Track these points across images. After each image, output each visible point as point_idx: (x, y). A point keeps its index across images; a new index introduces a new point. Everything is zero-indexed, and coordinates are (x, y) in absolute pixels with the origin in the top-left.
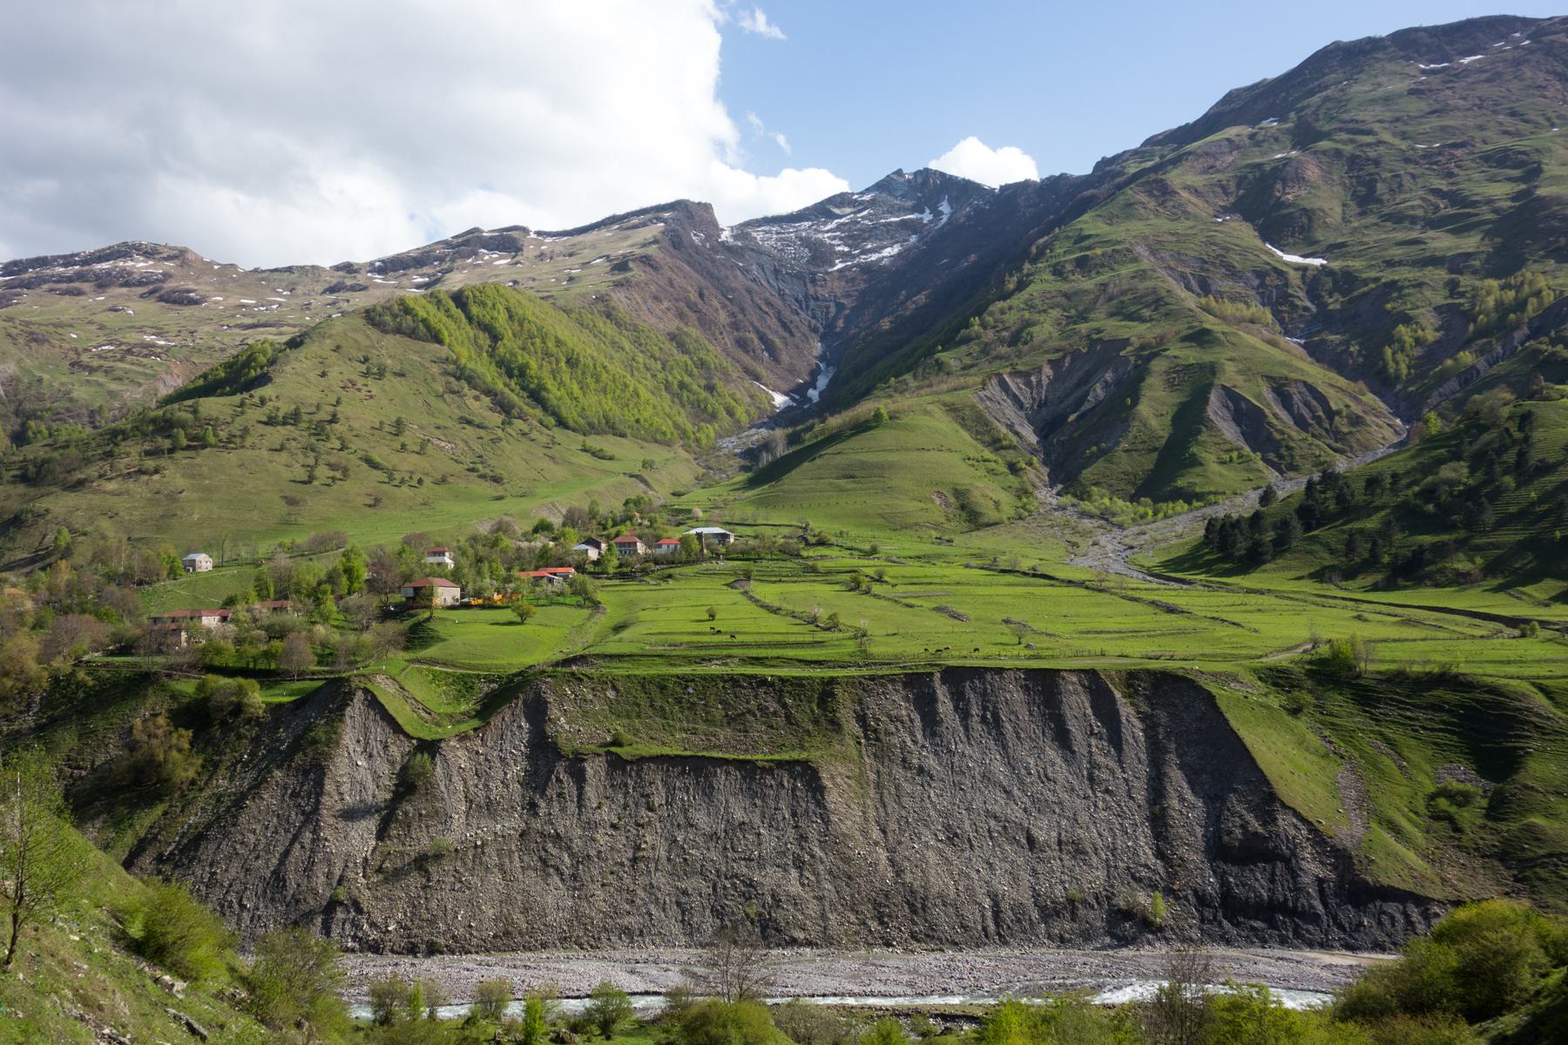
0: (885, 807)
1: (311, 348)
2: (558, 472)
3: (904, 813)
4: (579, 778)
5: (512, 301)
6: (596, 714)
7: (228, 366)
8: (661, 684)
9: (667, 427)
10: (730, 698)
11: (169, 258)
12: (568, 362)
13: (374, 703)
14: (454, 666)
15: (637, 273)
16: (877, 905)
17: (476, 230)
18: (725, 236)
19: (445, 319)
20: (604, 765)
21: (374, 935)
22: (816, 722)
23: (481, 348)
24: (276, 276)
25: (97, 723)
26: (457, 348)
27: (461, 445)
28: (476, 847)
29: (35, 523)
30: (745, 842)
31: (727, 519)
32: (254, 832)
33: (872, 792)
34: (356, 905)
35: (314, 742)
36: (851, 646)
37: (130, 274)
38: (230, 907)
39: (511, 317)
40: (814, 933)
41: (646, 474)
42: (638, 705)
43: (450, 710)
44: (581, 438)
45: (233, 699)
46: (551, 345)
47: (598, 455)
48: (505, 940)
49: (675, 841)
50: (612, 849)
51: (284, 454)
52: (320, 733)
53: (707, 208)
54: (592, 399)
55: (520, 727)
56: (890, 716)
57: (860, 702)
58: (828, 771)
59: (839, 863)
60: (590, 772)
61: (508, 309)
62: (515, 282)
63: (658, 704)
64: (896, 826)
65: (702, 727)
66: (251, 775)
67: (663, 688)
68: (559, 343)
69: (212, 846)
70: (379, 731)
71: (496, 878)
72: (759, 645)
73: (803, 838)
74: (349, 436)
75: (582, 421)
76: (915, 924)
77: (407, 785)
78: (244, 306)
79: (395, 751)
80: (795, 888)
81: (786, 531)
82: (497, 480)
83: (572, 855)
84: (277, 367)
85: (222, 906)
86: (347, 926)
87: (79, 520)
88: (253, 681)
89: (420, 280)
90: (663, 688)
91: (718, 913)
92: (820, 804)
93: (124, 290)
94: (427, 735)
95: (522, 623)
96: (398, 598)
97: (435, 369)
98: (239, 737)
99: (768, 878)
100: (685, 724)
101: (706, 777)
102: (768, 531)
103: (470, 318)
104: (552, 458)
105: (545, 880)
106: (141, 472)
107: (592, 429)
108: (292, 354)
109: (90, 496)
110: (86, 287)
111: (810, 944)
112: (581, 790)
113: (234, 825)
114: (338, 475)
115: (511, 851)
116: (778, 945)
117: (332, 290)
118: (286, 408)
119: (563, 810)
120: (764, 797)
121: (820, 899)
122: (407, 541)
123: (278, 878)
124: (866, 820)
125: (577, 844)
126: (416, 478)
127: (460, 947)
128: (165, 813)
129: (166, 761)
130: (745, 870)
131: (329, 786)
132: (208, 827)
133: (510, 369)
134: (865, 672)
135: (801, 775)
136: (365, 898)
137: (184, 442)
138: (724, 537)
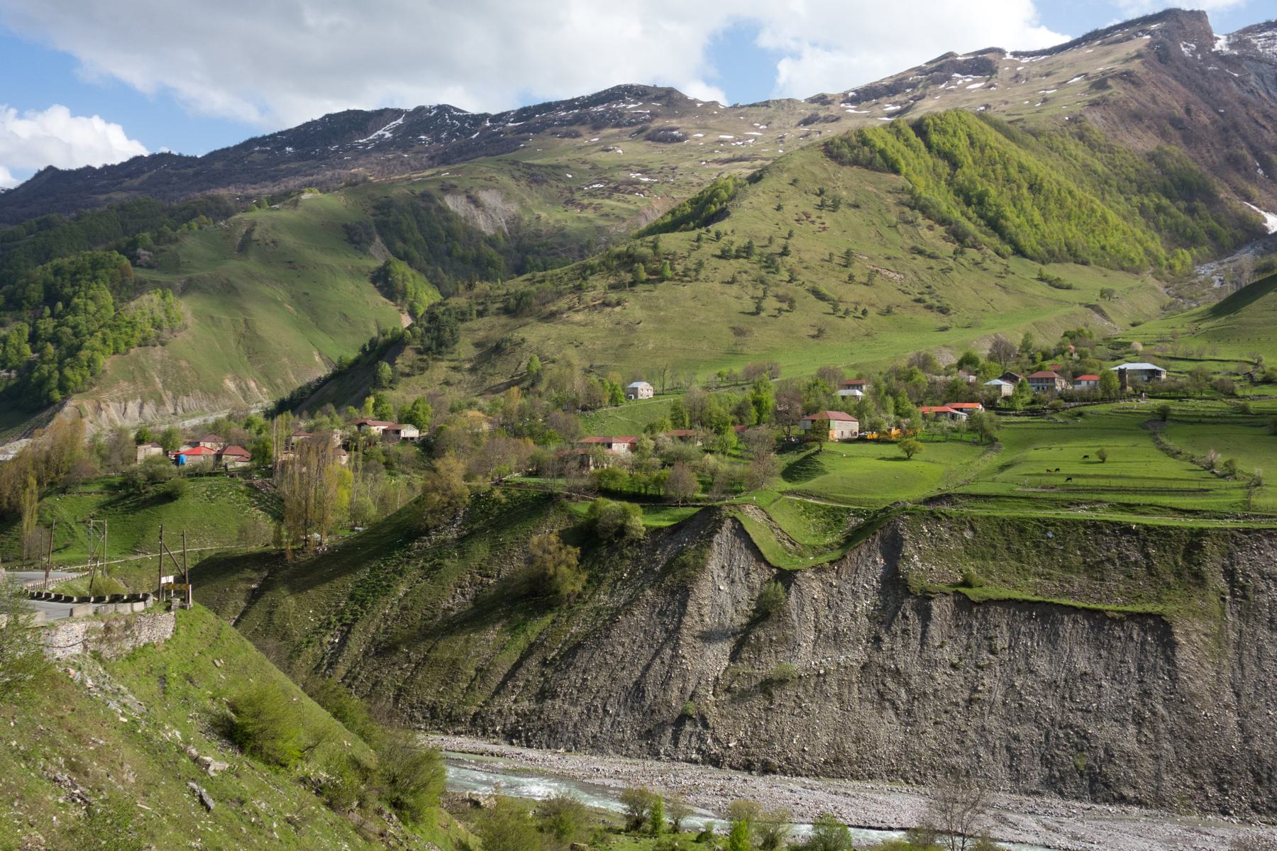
0: (1242, 667)
1: (769, 183)
2: (1010, 302)
3: (1262, 677)
4: (925, 615)
5: (974, 127)
6: (951, 553)
7: (694, 202)
8: (1021, 527)
9: (1136, 253)
10: (1091, 545)
11: (657, 99)
12: (1031, 187)
13: (740, 531)
14: (827, 499)
15: (1117, 91)
16: (1218, 770)
17: (951, 54)
18: (1221, 45)
19: (903, 148)
20: (951, 605)
21: (716, 750)
22: (1179, 575)
23: (939, 176)
24: (754, 110)
25: (506, 537)
26: (914, 178)
27: (911, 275)
28: (819, 675)
29: (513, 351)
30: (1085, 693)
31: (1170, 353)
32: (623, 645)
33: (1231, 653)
34: (703, 719)
35: (684, 565)
36: (1238, 496)
37: (621, 115)
38: (595, 711)
39: (972, 144)
40: (1145, 792)
41: (1103, 305)
42: (995, 547)
43: (814, 542)
44: (1038, 266)
45: (619, 521)
46: (1013, 171)
47: (1056, 284)
48: (835, 767)
49: (1013, 686)
50: (949, 688)
51: (735, 287)
52: (688, 558)
53: (1199, 16)
54: (1055, 226)
55: (875, 562)
56: (1261, 573)
57: (1230, 556)
58: (1183, 626)
59: (1183, 723)
60: (936, 610)
61: (970, 136)
62: (987, 106)
63: (1015, 547)
64: (1252, 691)
65: (1057, 572)
66: (628, 592)
67: (1021, 531)
68: (1022, 168)
69: (586, 655)
70: (743, 559)
71: (834, 706)
72: (1136, 491)
73: (1146, 694)
74: (798, 268)
75: (1041, 249)
76: (1258, 794)
77: (764, 612)
78: (722, 141)
79: (756, 579)
80: (1130, 745)
81: (1232, 367)
82: (944, 311)
83: (909, 691)
84: (735, 202)
85: (589, 710)
86: (694, 739)
87: (550, 349)
88: (637, 506)
89: (891, 108)
90: (1021, 531)
91: (1047, 762)
92: (1170, 660)
93: (616, 130)
94: (786, 566)
95: (908, 459)
96: (796, 431)
97: (890, 200)
98: (622, 557)
99: (1104, 732)
100: (1040, 569)
101: (1053, 624)
102: (1214, 367)
103: (929, 147)
104: (1004, 288)
105: (880, 713)
106: (606, 304)
107: (1052, 257)
108: (751, 189)
109: (560, 327)
110: (582, 130)
111: (1139, 803)
112: (925, 627)
113: (607, 637)
114: (785, 306)
115: (851, 682)
116: (1105, 801)
117: (806, 122)
118: (740, 241)
119: (905, 646)
120: (1110, 649)
121: (1156, 758)
122: (823, 374)
123: (638, 689)
124: (1219, 680)
125: (915, 681)
126: (860, 309)
127: (792, 769)
128: (554, 622)
129: (556, 575)
130: (1080, 722)
131: (691, 608)
132: (586, 637)
133: (969, 197)
134: (1242, 524)
135: (1152, 629)
136: (712, 714)
137: (644, 276)
138: (1153, 374)
